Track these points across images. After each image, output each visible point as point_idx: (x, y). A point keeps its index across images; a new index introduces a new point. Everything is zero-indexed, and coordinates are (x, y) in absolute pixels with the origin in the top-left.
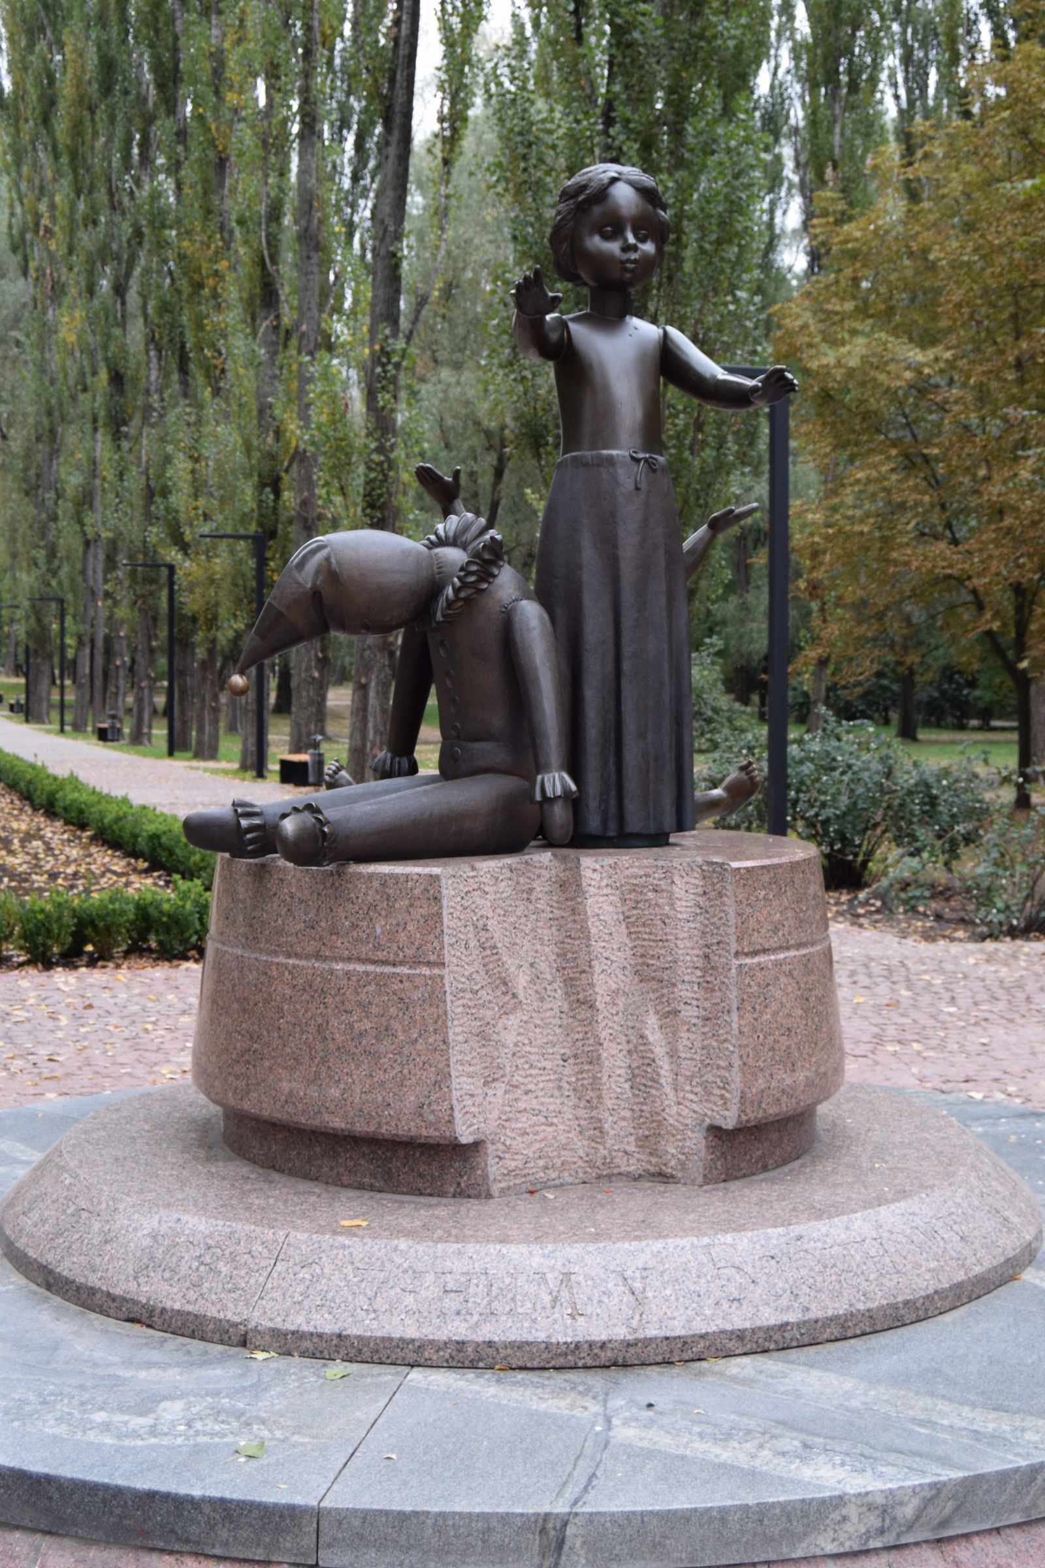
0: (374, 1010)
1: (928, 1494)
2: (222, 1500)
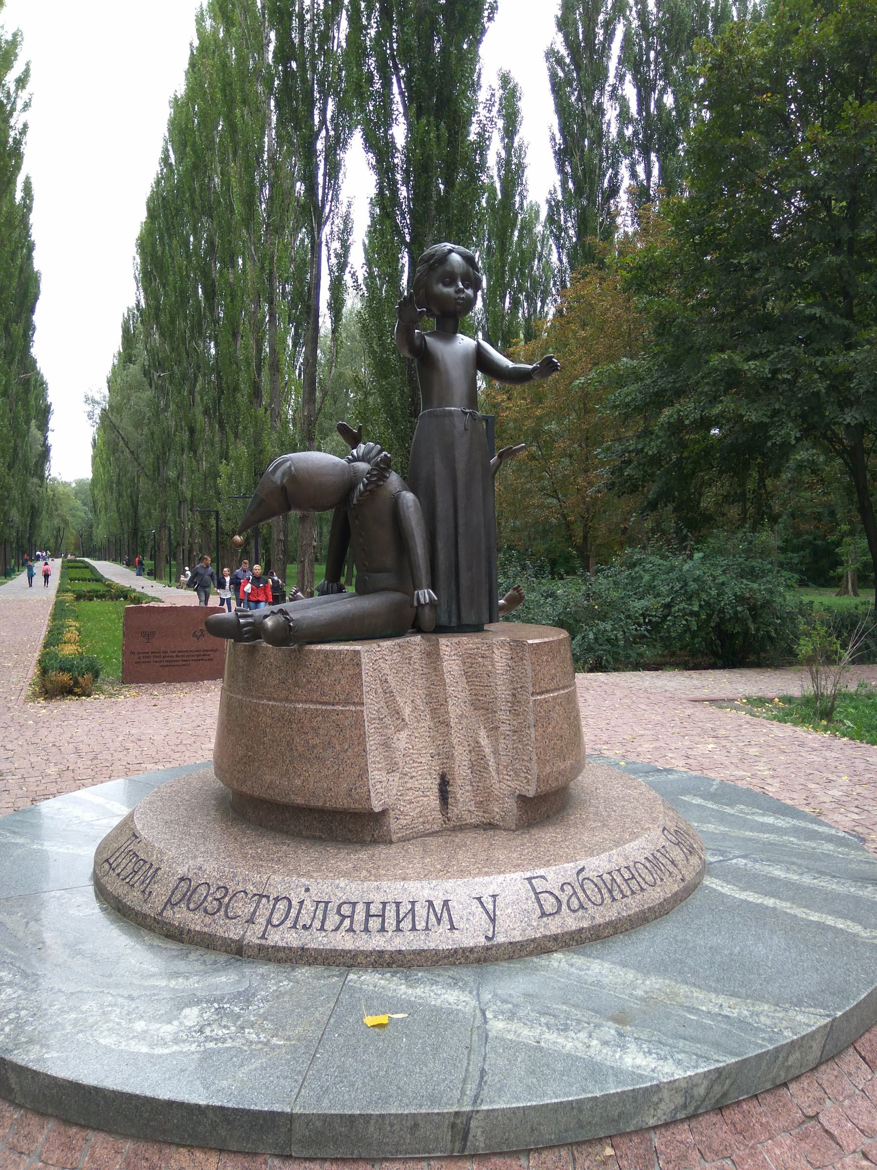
0: (321, 732)
1: (713, 1076)
2: (222, 1108)
